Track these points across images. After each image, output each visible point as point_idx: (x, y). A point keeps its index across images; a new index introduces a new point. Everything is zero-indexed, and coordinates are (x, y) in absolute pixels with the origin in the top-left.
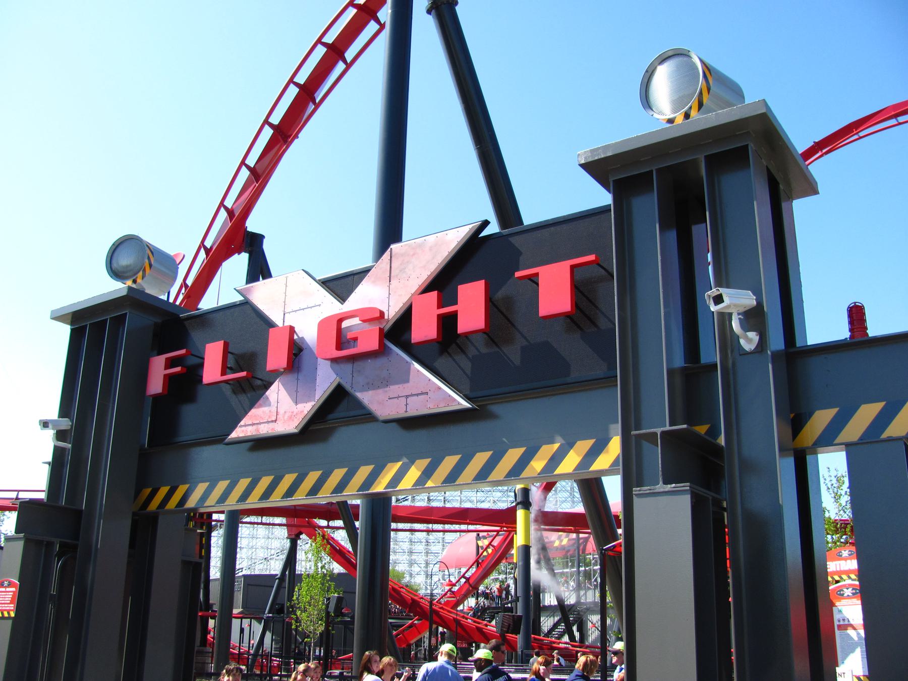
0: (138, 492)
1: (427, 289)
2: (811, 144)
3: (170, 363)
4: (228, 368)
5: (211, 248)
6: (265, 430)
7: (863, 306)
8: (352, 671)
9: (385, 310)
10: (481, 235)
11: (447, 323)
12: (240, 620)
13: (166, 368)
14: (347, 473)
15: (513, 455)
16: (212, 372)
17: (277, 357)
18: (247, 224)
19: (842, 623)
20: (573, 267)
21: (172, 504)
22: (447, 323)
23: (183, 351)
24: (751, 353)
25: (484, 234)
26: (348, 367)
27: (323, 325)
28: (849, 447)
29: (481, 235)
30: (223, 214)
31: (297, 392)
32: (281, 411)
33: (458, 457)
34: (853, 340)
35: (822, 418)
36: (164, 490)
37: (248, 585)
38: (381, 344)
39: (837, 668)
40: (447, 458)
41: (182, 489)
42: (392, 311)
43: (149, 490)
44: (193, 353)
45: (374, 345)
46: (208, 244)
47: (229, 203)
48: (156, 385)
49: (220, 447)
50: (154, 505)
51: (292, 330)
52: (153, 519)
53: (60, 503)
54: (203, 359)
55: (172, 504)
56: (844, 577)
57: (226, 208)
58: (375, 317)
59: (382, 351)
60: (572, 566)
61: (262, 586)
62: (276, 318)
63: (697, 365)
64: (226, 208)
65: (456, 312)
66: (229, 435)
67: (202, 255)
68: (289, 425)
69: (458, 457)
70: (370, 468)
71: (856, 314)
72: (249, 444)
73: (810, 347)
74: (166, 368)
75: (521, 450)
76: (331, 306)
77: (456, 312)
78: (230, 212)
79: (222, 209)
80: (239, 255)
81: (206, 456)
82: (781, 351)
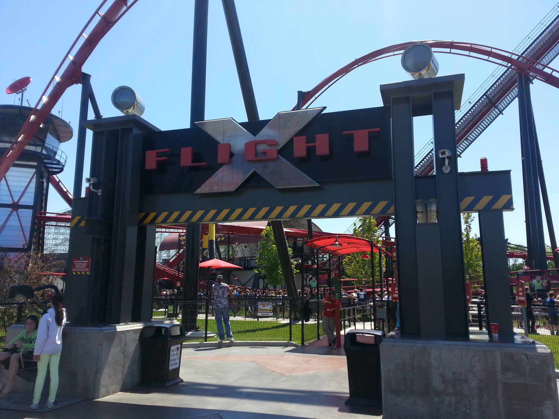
2: (542, 160)
3: (158, 155)
7: (486, 159)
11: (311, 150)
14: (282, 210)
15: (176, 214)
17: (222, 156)
22: (311, 150)
24: (445, 174)
25: (323, 112)
28: (479, 211)
33: (325, 205)
34: (483, 172)
36: (152, 215)
39: (337, 409)
40: (187, 212)
42: (282, 142)
51: (229, 146)
58: (271, 143)
59: (277, 159)
60: (333, 262)
63: (436, 176)
65: (315, 146)
69: (325, 205)
70: (191, 212)
71: (484, 162)
75: (282, 208)
76: (249, 137)
77: (315, 146)
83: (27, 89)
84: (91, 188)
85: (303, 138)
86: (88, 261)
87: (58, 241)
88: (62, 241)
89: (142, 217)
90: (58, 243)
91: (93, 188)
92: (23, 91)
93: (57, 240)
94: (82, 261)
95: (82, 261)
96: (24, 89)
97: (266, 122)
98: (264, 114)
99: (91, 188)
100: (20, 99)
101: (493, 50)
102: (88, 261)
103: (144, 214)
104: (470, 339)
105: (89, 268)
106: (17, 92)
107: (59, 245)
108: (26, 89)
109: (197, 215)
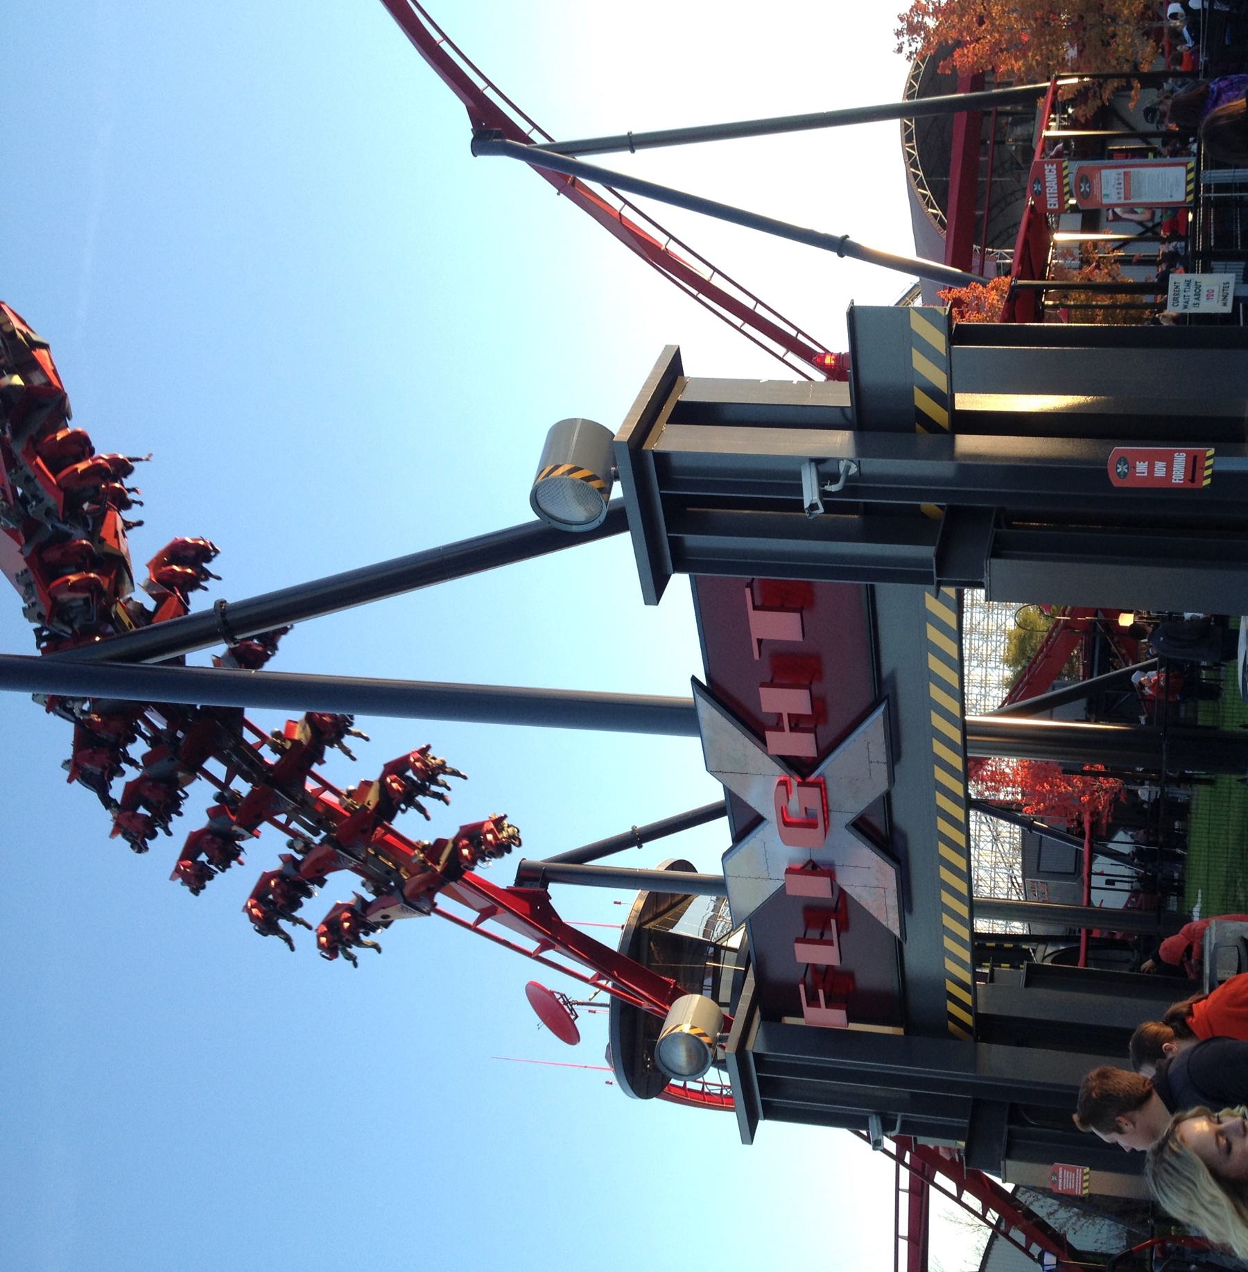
0: (952, 1036)
1: (761, 740)
4: (821, 938)
5: (538, 941)
6: (893, 900)
8: (1082, 1177)
9: (777, 780)
10: (705, 683)
12: (1093, 876)
13: (819, 1006)
16: (825, 956)
17: (818, 888)
18: (503, 886)
19: (1123, 196)
20: (755, 608)
21: (967, 998)
22: (797, 724)
23: (802, 987)
26: (834, 816)
27: (786, 841)
29: (705, 683)
30: (489, 925)
31: (856, 866)
32: (875, 883)
35: (923, 402)
36: (952, 1007)
37: (1038, 870)
38: (812, 785)
41: (951, 987)
42: (777, 772)
43: (950, 1024)
44: (802, 976)
45: (815, 792)
46: (532, 945)
47: (470, 916)
48: (834, 1018)
49: (906, 947)
50: (968, 1019)
52: (978, 1018)
53: (966, 1126)
54: (808, 964)
55: (967, 998)
56: (1066, 181)
57: (479, 920)
59: (821, 785)
61: (1040, 851)
62: (773, 887)
64: (479, 920)
66: (895, 937)
67: (550, 955)
68: (887, 874)
72: (906, 914)
73: (854, 403)
74: (819, 1006)
77: (789, 715)
78: (485, 914)
79: (481, 926)
80: (551, 898)
81: (915, 959)
82: (855, 434)
83: (563, 992)
84: (894, 1134)
85: (770, 736)
86: (1061, 1168)
87: (982, 833)
88: (983, 823)
89: (956, 1024)
90: (989, 833)
91: (893, 1129)
92: (567, 1002)
93: (979, 836)
94: (1060, 1177)
95: (1060, 1177)
96: (561, 1000)
97: (727, 791)
98: (714, 793)
99: (894, 1134)
100: (590, 1011)
101: (904, 1230)
102: (1061, 1168)
103: (949, 1022)
104: (1204, 1117)
105: (1172, 454)
106: (573, 1017)
107: (996, 831)
108: (562, 995)
109: (950, 904)
